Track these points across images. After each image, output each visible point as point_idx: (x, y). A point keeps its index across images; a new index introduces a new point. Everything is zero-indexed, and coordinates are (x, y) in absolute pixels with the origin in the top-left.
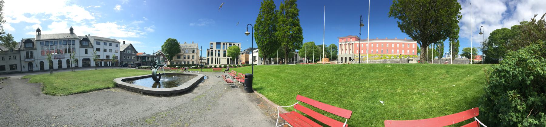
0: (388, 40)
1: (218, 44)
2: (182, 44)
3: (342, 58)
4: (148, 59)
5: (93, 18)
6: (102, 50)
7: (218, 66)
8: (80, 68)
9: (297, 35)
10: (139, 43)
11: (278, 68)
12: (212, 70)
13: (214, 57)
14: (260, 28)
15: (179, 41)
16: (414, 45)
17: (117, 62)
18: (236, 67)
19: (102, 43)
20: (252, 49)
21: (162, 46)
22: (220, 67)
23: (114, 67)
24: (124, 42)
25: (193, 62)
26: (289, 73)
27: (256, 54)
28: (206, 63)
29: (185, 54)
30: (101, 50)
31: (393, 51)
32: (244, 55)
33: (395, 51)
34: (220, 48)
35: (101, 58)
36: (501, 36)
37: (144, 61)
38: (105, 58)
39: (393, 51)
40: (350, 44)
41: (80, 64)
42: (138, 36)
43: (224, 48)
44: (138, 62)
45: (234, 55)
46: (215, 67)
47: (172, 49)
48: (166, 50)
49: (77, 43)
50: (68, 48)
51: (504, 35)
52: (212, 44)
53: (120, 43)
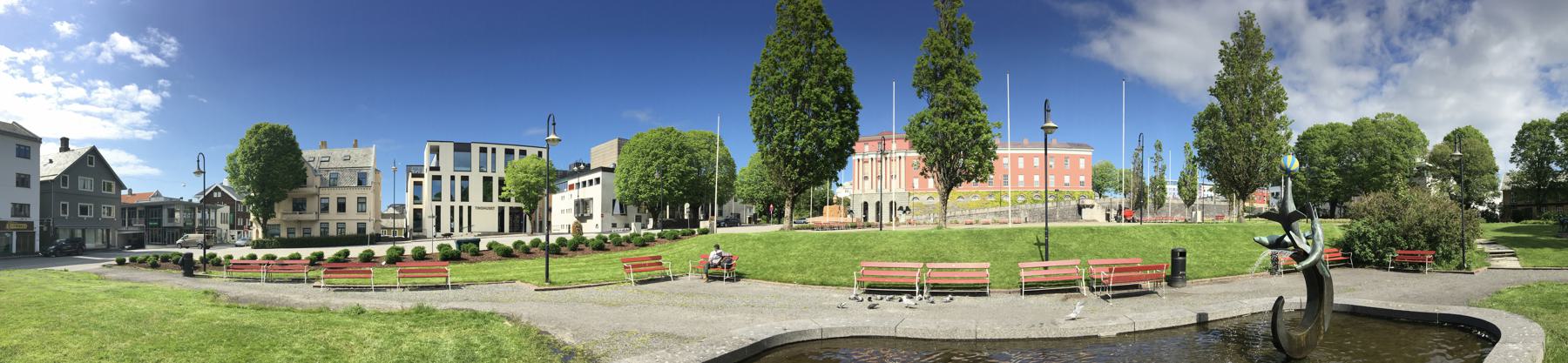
1: (462, 148)
2: (310, 153)
3: (866, 205)
16: (1082, 161)
17: (26, 236)
25: (361, 228)
27: (594, 193)
29: (324, 193)
33: (1029, 181)
34: (467, 165)
36: (1327, 146)
37: (150, 230)
40: (865, 162)
47: (275, 171)
51: (1335, 142)
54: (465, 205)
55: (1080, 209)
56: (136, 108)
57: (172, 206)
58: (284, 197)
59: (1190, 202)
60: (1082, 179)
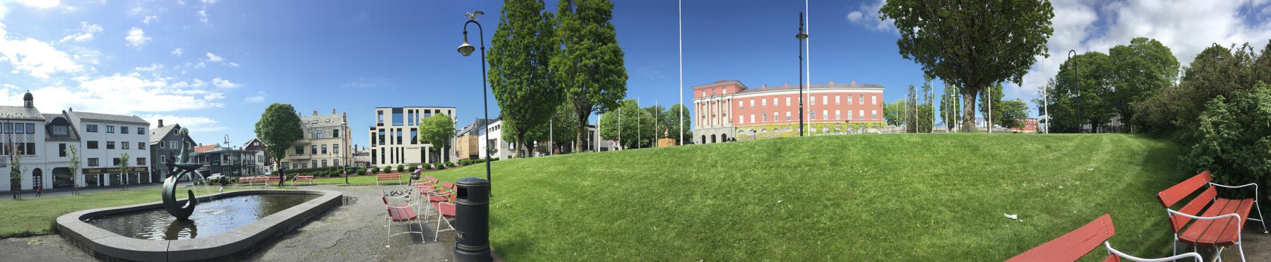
0: (836, 86)
1: (397, 111)
3: (704, 138)
5: (79, 68)
6: (102, 145)
7: (395, 167)
8: (48, 191)
10: (206, 120)
12: (375, 178)
13: (387, 146)
15: (298, 111)
16: (874, 98)
18: (442, 168)
19: (102, 128)
20: (484, 123)
21: (257, 125)
22: (401, 169)
23: (148, 184)
24: (161, 121)
25: (336, 162)
26: (604, 176)
27: (496, 135)
28: (368, 164)
29: (313, 143)
31: (825, 113)
32: (467, 136)
33: (832, 115)
34: (401, 122)
35: (102, 165)
36: (1087, 71)
37: (224, 167)
38: (111, 165)
39: (825, 113)
40: (723, 102)
41: (48, 181)
42: (201, 105)
43: (410, 121)
45: (440, 139)
46: (388, 170)
47: (282, 129)
48: (267, 134)
49: (40, 130)
50: (25, 142)
51: (1094, 67)
52: (380, 113)
53: (148, 125)
54: (400, 147)
57: (228, 153)
58: (288, 147)
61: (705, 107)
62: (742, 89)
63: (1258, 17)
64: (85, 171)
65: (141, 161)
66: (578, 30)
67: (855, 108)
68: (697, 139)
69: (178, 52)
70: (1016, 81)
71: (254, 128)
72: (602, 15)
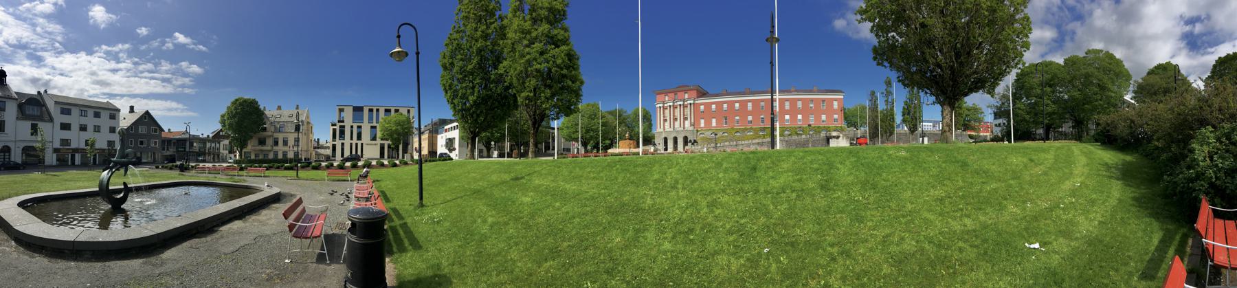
1: (358, 110)
3: (666, 140)
4: (191, 145)
9: (565, 72)
10: (174, 105)
11: (507, 169)
12: (323, 174)
13: (347, 141)
14: (456, 62)
16: (835, 103)
27: (455, 134)
29: (276, 135)
30: (72, 127)
33: (794, 117)
34: (362, 120)
35: (74, 145)
37: (181, 153)
38: (83, 146)
40: (685, 106)
42: (169, 89)
43: (370, 119)
44: (169, 153)
47: (246, 122)
48: (230, 125)
52: (341, 110)
54: (359, 143)
55: (828, 139)
56: (186, 75)
57: (193, 139)
59: (913, 129)
60: (836, 116)
61: (667, 112)
62: (703, 94)
63: (1199, 43)
64: (56, 150)
65: (111, 143)
66: (529, 32)
67: (818, 113)
68: (659, 141)
69: (143, 31)
70: (989, 93)
71: (219, 119)
72: (556, 16)
